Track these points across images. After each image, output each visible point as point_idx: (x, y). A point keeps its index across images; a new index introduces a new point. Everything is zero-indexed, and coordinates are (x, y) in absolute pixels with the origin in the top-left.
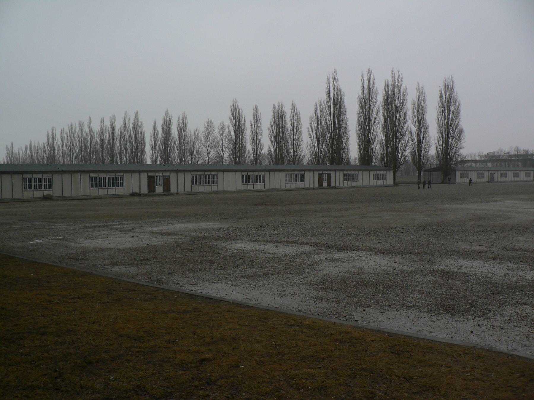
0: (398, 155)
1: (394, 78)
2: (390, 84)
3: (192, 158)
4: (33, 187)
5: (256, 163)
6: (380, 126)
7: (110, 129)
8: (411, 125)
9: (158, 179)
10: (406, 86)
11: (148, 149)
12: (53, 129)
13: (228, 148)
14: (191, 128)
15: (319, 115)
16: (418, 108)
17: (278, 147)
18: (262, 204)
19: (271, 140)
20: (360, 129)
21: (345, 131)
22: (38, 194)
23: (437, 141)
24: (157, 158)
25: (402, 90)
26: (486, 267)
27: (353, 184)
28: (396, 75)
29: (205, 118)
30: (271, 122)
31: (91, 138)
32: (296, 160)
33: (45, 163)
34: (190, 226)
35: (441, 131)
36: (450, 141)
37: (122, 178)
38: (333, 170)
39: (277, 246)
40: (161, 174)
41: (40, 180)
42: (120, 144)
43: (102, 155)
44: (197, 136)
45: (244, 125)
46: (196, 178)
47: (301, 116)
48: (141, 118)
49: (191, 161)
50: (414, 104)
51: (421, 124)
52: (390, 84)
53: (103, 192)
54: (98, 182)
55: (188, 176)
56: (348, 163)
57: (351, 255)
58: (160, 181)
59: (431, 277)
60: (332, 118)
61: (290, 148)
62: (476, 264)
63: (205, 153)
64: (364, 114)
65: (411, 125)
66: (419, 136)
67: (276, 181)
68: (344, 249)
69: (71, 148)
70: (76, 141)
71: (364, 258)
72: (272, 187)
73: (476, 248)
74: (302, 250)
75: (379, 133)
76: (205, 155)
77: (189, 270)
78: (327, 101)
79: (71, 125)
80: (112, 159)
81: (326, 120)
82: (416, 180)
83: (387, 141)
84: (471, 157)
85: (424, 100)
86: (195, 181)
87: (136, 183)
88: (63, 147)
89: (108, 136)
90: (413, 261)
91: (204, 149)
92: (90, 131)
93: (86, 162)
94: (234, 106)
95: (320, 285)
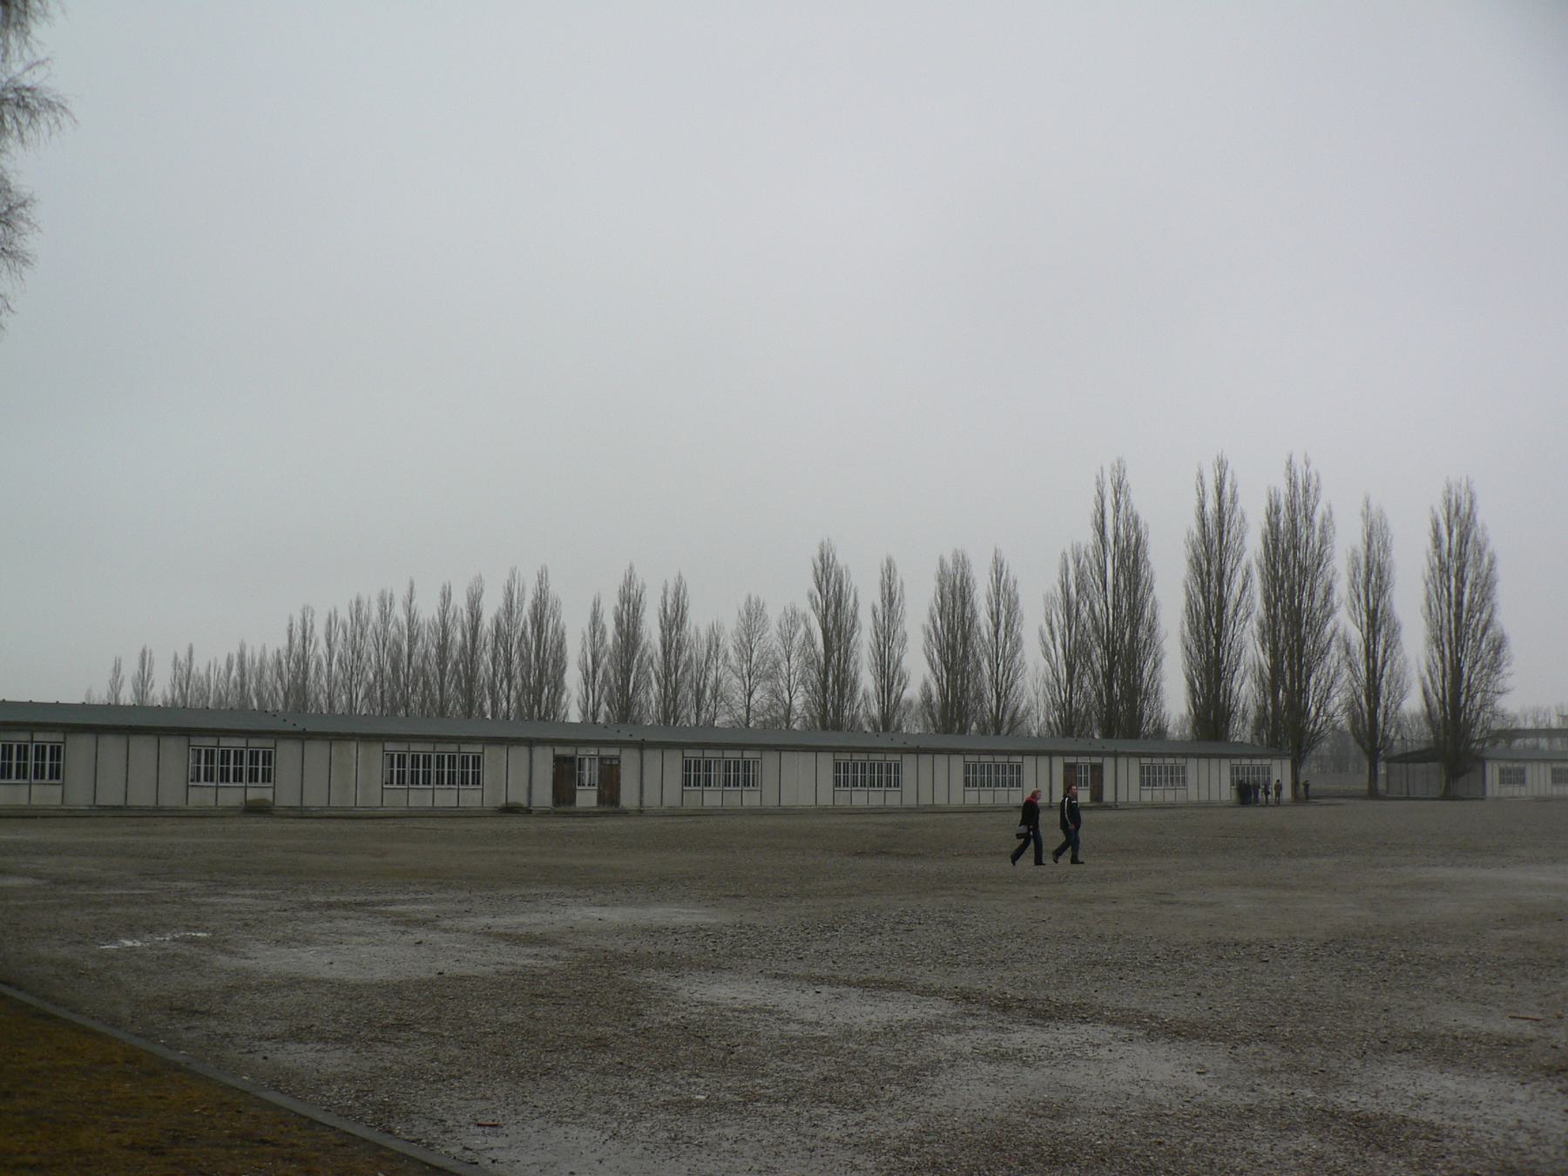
0: (1306, 712)
1: (1292, 484)
2: (1283, 501)
3: (699, 708)
4: (217, 775)
5: (886, 728)
6: (1255, 626)
7: (466, 616)
8: (1345, 623)
9: (583, 770)
10: (1329, 507)
11: (573, 678)
12: (306, 611)
13: (803, 682)
14: (698, 622)
15: (1073, 590)
16: (1369, 573)
17: (952, 682)
18: (880, 852)
19: (931, 662)
20: (1195, 631)
21: (1150, 636)
22: (232, 795)
23: (1425, 672)
24: (599, 704)
25: (1317, 519)
26: (1516, 1106)
27: (1170, 797)
28: (1299, 474)
29: (737, 587)
30: (931, 609)
31: (412, 640)
32: (1003, 722)
33: (280, 707)
34: (616, 915)
35: (1438, 641)
36: (1466, 670)
37: (477, 761)
38: (1109, 754)
39: (839, 997)
40: (593, 751)
41: (239, 756)
42: (494, 660)
43: (441, 689)
44: (714, 644)
45: (854, 617)
46: (697, 768)
47: (1019, 590)
48: (554, 589)
49: (698, 715)
50: (1354, 559)
51: (1376, 620)
52: (1283, 501)
53: (420, 797)
54: (408, 769)
55: (674, 761)
56: (1160, 732)
57: (1064, 1039)
58: (590, 771)
59: (1305, 1137)
60: (1110, 600)
61: (987, 685)
62: (1480, 1088)
63: (739, 697)
64: (1205, 590)
65: (1345, 623)
66: (1370, 654)
67: (937, 783)
68: (1051, 1018)
69: (353, 669)
70: (369, 648)
71: (1103, 1052)
72: (926, 800)
73: (1497, 1028)
74: (913, 1013)
75: (1250, 644)
76: (736, 700)
77: (508, 1072)
78: (1095, 548)
79: (358, 603)
80: (471, 703)
81: (1092, 608)
82: (1362, 784)
83: (1276, 669)
84: (1535, 721)
85: (1385, 548)
86: (695, 776)
87: (521, 777)
88: (330, 664)
89: (459, 637)
90: (1262, 1072)
91: (736, 681)
92: (411, 620)
93: (395, 709)
94: (822, 559)
95: (907, 1153)
